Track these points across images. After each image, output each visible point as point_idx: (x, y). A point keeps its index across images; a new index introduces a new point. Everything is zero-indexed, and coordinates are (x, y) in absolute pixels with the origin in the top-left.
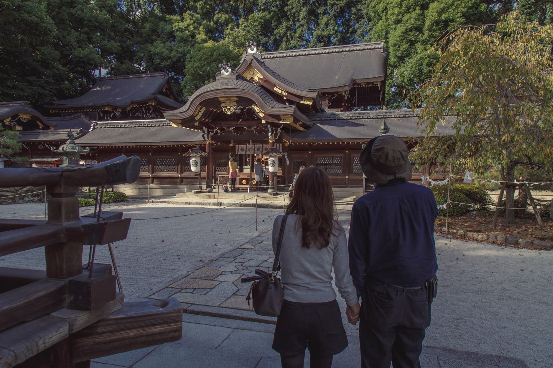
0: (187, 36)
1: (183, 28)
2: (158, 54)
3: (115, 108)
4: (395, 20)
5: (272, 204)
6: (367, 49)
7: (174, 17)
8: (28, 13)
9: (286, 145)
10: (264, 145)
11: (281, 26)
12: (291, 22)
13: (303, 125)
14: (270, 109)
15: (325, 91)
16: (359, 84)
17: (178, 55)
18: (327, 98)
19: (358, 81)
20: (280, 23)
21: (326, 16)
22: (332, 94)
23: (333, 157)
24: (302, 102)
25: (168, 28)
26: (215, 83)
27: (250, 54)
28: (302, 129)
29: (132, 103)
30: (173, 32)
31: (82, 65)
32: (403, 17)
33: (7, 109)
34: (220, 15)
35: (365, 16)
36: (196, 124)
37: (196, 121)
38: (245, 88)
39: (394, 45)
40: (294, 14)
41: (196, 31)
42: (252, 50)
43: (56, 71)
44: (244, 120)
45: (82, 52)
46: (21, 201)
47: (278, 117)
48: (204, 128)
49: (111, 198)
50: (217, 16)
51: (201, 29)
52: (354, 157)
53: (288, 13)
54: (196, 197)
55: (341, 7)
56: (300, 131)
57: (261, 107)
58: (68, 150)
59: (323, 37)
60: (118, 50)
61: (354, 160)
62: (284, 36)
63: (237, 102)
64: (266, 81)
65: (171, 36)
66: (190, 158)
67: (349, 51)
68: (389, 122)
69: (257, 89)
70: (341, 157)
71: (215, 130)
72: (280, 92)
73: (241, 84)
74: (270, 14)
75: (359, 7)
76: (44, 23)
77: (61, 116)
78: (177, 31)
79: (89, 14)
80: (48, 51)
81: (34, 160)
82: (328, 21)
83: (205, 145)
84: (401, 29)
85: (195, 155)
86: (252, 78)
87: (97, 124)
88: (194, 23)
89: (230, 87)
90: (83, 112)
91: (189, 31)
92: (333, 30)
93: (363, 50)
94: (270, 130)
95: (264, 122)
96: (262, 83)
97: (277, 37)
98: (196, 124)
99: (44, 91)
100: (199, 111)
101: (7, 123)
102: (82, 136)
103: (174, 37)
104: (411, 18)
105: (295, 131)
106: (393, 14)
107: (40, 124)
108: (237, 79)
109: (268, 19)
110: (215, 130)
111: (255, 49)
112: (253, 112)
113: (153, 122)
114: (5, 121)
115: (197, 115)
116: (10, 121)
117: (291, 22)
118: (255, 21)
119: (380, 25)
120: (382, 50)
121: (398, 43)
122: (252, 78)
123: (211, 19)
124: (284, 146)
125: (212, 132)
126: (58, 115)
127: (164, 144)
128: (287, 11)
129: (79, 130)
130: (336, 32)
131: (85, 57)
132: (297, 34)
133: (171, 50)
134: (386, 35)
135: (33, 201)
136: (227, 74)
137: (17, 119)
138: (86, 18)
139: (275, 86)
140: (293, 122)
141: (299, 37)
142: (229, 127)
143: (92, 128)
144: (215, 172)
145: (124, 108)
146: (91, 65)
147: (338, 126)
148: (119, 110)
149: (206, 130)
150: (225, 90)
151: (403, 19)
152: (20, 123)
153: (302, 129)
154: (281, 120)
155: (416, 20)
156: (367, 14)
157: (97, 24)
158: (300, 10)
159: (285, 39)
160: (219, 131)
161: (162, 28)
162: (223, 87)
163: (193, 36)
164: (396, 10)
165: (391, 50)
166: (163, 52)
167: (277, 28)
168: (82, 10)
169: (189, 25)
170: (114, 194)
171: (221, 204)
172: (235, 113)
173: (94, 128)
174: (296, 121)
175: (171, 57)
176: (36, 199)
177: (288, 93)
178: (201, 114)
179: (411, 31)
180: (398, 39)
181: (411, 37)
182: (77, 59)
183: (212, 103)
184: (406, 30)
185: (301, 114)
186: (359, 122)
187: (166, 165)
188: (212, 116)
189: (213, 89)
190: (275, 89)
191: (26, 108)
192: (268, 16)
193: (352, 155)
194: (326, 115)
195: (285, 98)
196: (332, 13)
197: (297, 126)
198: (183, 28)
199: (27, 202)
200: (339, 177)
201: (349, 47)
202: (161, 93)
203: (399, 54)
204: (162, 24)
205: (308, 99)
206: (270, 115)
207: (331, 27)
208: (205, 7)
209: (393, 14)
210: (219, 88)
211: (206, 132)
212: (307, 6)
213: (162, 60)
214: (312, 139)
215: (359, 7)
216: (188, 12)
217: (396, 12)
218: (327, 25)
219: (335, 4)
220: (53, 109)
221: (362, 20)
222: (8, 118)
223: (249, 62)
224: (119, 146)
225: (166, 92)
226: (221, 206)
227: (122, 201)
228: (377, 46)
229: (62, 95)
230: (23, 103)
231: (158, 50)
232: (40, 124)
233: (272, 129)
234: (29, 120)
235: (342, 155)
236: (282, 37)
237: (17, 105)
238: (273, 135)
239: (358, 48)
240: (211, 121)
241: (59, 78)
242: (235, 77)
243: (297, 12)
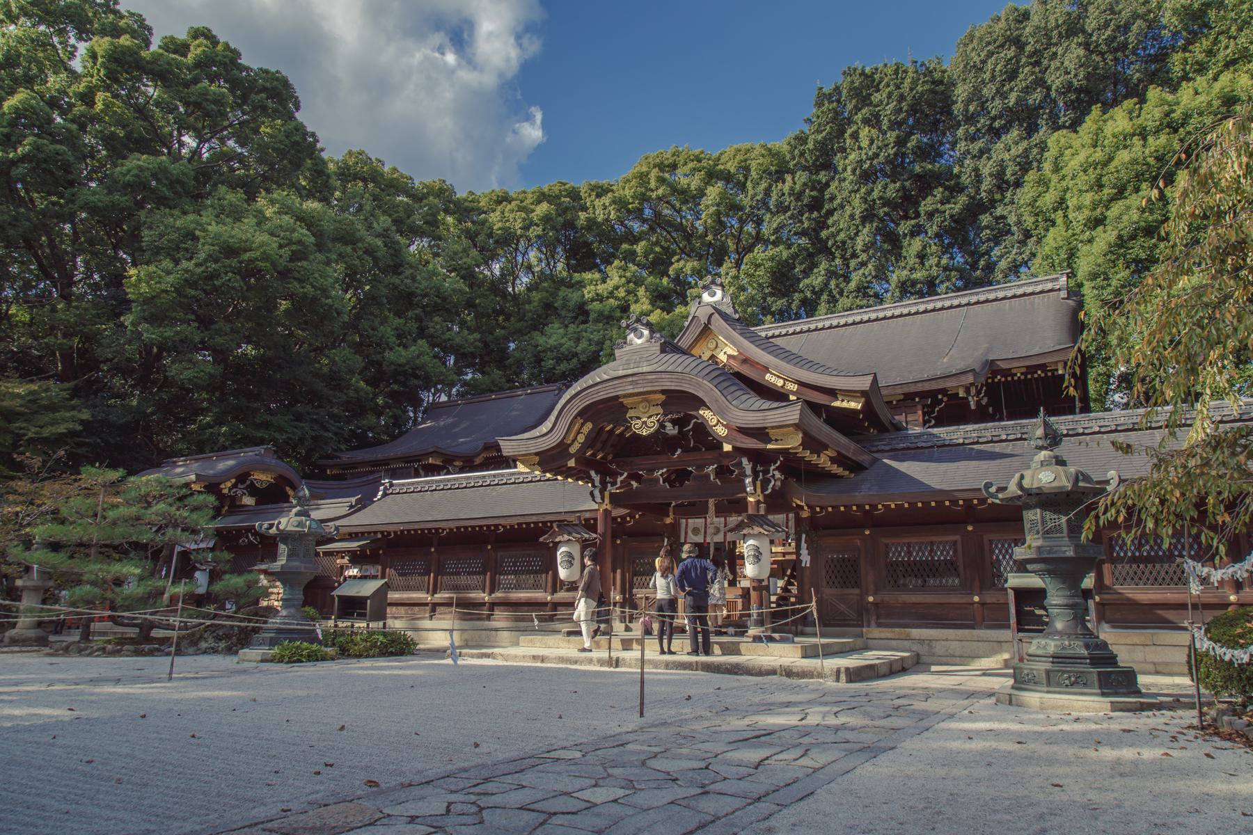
0: (613, 310)
1: (605, 294)
2: (550, 349)
4: (1089, 220)
5: (750, 664)
6: (1024, 295)
7: (588, 276)
8: (300, 281)
9: (805, 514)
11: (815, 270)
12: (838, 261)
13: (840, 460)
14: (741, 413)
15: (912, 389)
17: (593, 348)
18: (920, 407)
19: (1003, 365)
20: (814, 265)
21: (918, 238)
22: (932, 394)
23: (932, 543)
24: (837, 404)
25: (574, 297)
26: (611, 364)
28: (836, 469)
30: (585, 303)
31: (403, 379)
32: (1107, 209)
33: (231, 463)
34: (682, 263)
35: (1014, 229)
36: (572, 463)
37: (571, 456)
38: (679, 370)
39: (1094, 276)
40: (844, 243)
41: (631, 298)
42: (714, 295)
43: (352, 393)
44: (686, 450)
45: (403, 353)
46: (191, 650)
47: (760, 433)
48: (593, 473)
49: (374, 645)
50: (675, 265)
51: (641, 292)
52: (991, 542)
53: (830, 243)
54: (565, 644)
55: (952, 216)
56: (842, 477)
57: (720, 412)
58: (289, 528)
59: (914, 283)
60: (476, 347)
61: (992, 552)
62: (822, 290)
63: (663, 405)
64: (746, 361)
65: (581, 312)
66: (556, 545)
67: (978, 303)
69: (707, 370)
70: (955, 543)
71: (620, 479)
72: (780, 383)
73: (673, 362)
74: (789, 248)
75: (999, 211)
76: (327, 298)
78: (593, 300)
79: (424, 284)
80: (343, 355)
82: (924, 247)
83: (595, 520)
84: (1105, 237)
85: (566, 537)
86: (713, 357)
87: (392, 485)
88: (628, 282)
89: (645, 369)
90: (386, 470)
91: (616, 298)
92: (938, 265)
93: (1014, 297)
94: (748, 471)
95: (727, 448)
96: (736, 366)
97: (809, 294)
98: (572, 463)
99: (322, 433)
100: (579, 433)
101: (225, 491)
103: (586, 313)
104: (1128, 208)
105: (815, 476)
106: (1079, 208)
108: (663, 351)
109: (786, 261)
111: (719, 293)
112: (702, 430)
116: (235, 486)
117: (838, 261)
118: (757, 266)
119: (1054, 238)
120: (1063, 294)
121: (1102, 269)
122: (713, 357)
123: (664, 273)
124: (798, 520)
125: (614, 484)
127: (515, 521)
128: (828, 239)
129: (353, 500)
130: (946, 269)
131: (408, 363)
132: (853, 285)
133: (578, 340)
134: (1069, 258)
135: (215, 651)
136: (639, 341)
138: (418, 291)
139: (766, 369)
141: (858, 289)
142: (651, 471)
144: (631, 588)
146: (416, 377)
147: (939, 460)
149: (597, 479)
150: (634, 378)
151: (1108, 213)
152: (253, 490)
153: (836, 469)
154: (769, 441)
155: (1143, 211)
156: (1019, 223)
157: (439, 301)
158: (856, 234)
159: (825, 297)
161: (564, 299)
162: (630, 372)
163: (625, 309)
164: (1088, 198)
165: (1087, 290)
166: (561, 345)
167: (807, 276)
168: (413, 278)
169: (617, 288)
170: (385, 634)
171: (617, 663)
173: (385, 495)
174: (812, 443)
175: (576, 355)
176: (222, 645)
177: (801, 384)
178: (581, 438)
179: (1133, 237)
180: (1100, 260)
181: (1138, 250)
182: (393, 367)
183: (608, 411)
184: (1120, 237)
186: (997, 448)
187: (523, 572)
188: (607, 446)
189: (606, 377)
190: (768, 377)
191: (267, 460)
192: (785, 254)
193: (986, 537)
194: (907, 437)
196: (933, 229)
197: (823, 461)
198: (605, 294)
199: (205, 652)
200: (954, 599)
201: (977, 294)
203: (1107, 294)
204: (563, 292)
205: (850, 394)
206: (743, 431)
207: (933, 261)
208: (652, 251)
209: (1079, 208)
210: (621, 373)
211: (597, 483)
212: (871, 222)
213: (559, 360)
214: (864, 494)
215: (999, 211)
216: (616, 263)
217: (1087, 203)
218: (922, 257)
219: (937, 210)
220: (331, 467)
221: (1009, 237)
223: (704, 320)
224: (422, 530)
226: (617, 666)
227: (401, 653)
228: (1049, 286)
229: (363, 442)
230: (261, 449)
231: (552, 342)
235: (958, 538)
236: (818, 294)
237: (249, 454)
238: (758, 483)
239: (1001, 294)
240: (610, 457)
241: (359, 408)
242: (656, 347)
243: (851, 238)
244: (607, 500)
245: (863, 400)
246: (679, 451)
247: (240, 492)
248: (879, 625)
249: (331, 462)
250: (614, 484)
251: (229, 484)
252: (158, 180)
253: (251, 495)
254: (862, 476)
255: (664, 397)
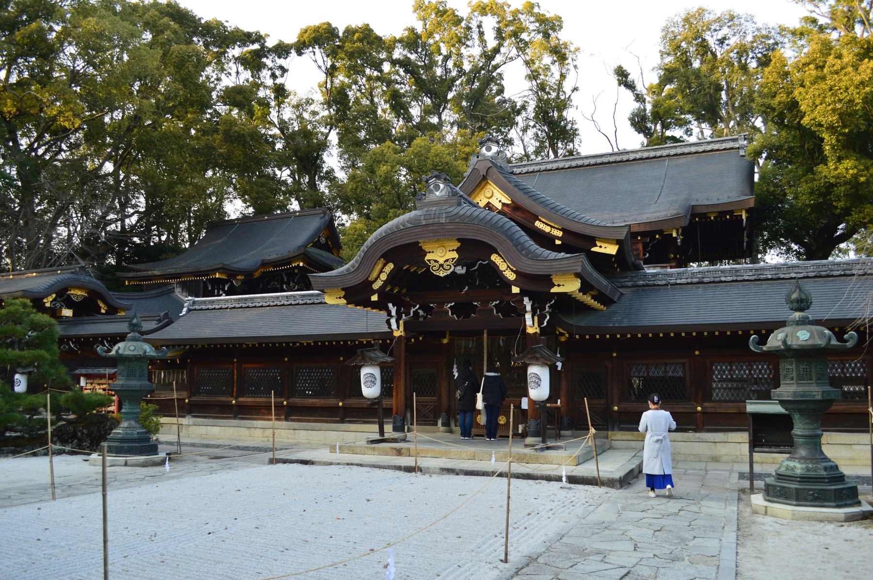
3: (232, 274)
6: (712, 151)
10: (661, 374)
14: (530, 262)
16: (704, 216)
27: (486, 159)
29: (264, 264)
36: (375, 298)
37: (374, 292)
48: (390, 305)
56: (596, 310)
68: (810, 287)
72: (547, 229)
77: (142, 291)
81: (83, 371)
94: (529, 308)
95: (515, 290)
101: (48, 305)
102: (167, 324)
107: (101, 305)
110: (413, 310)
112: (494, 267)
113: (294, 296)
114: (45, 301)
115: (376, 279)
116: (54, 300)
125: (407, 314)
126: (139, 289)
137: (65, 297)
139: (537, 218)
140: (580, 290)
143: (185, 310)
145: (248, 274)
148: (239, 277)
152: (70, 304)
160: (421, 312)
172: (453, 273)
178: (384, 277)
185: (596, 275)
195: (558, 242)
197: (587, 299)
202: (317, 245)
211: (394, 313)
220: (130, 279)
222: (50, 295)
225: (327, 242)
232: (101, 305)
233: (532, 306)
234: (85, 298)
238: (536, 318)
244: (402, 328)
245: (617, 247)
246: (467, 288)
247: (58, 305)
248: (621, 429)
249: (131, 275)
250: (407, 314)
251: (50, 299)
252: (731, 97)
253: (69, 308)
254: (613, 308)
255: (459, 244)
